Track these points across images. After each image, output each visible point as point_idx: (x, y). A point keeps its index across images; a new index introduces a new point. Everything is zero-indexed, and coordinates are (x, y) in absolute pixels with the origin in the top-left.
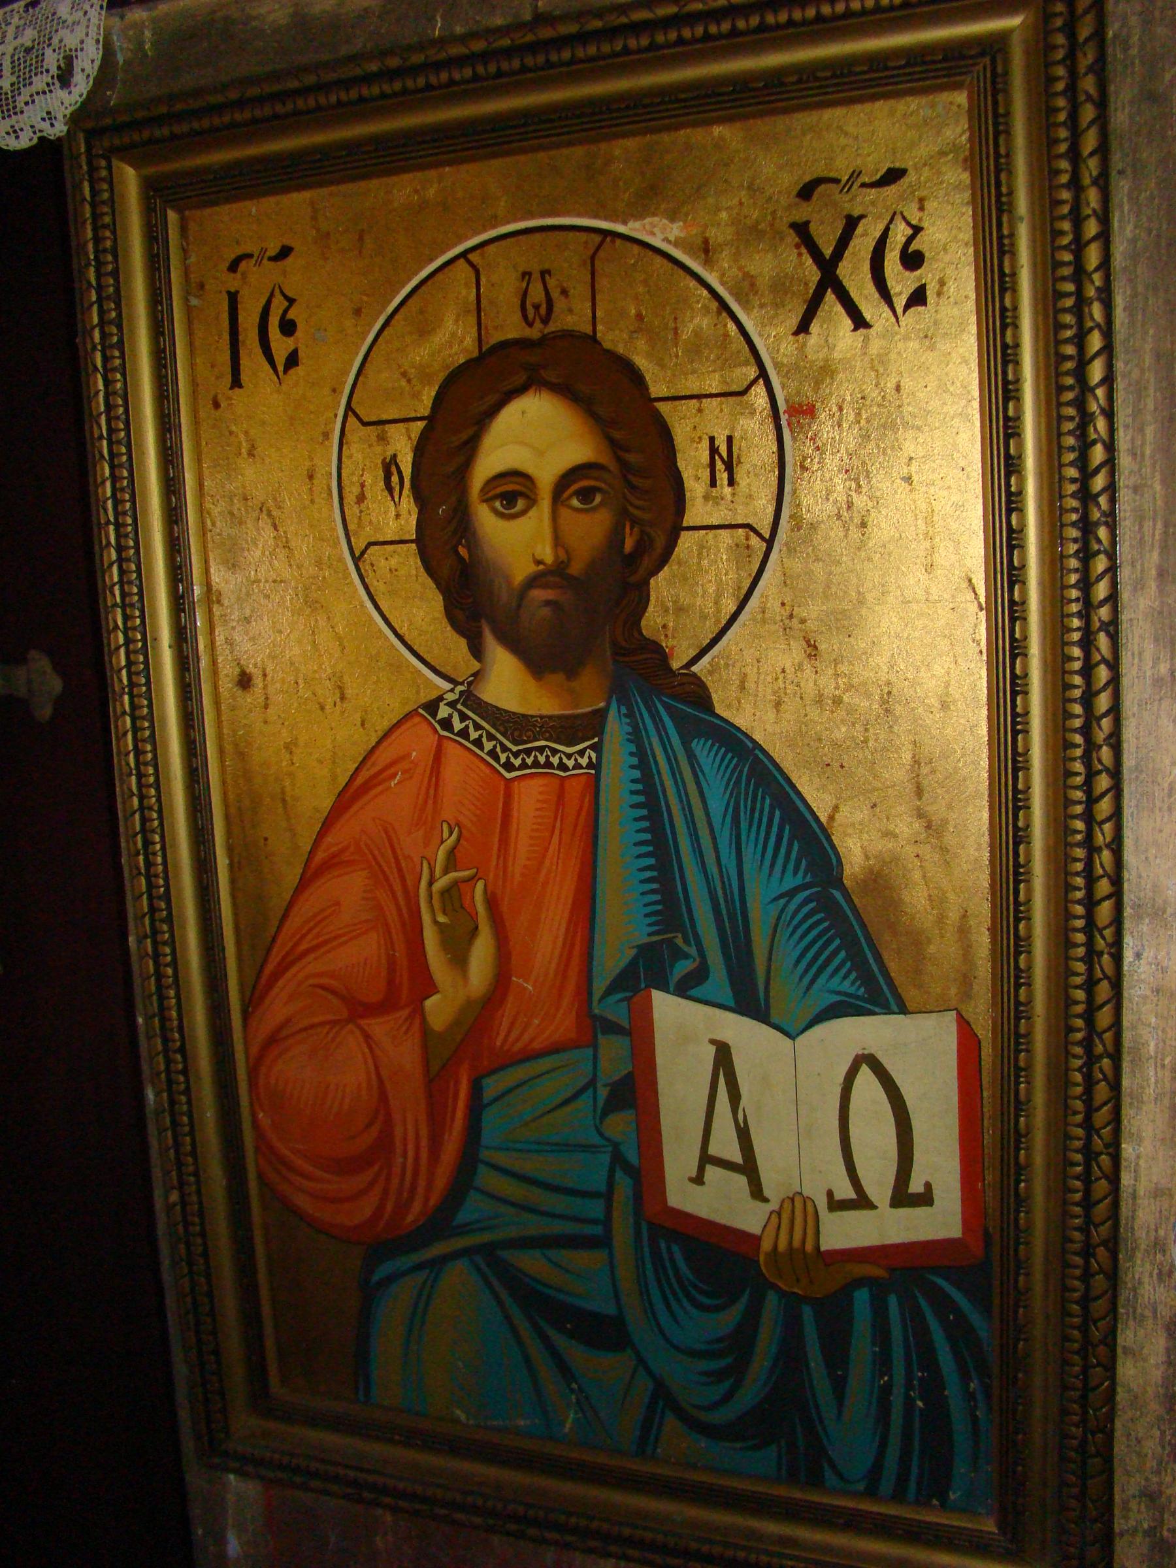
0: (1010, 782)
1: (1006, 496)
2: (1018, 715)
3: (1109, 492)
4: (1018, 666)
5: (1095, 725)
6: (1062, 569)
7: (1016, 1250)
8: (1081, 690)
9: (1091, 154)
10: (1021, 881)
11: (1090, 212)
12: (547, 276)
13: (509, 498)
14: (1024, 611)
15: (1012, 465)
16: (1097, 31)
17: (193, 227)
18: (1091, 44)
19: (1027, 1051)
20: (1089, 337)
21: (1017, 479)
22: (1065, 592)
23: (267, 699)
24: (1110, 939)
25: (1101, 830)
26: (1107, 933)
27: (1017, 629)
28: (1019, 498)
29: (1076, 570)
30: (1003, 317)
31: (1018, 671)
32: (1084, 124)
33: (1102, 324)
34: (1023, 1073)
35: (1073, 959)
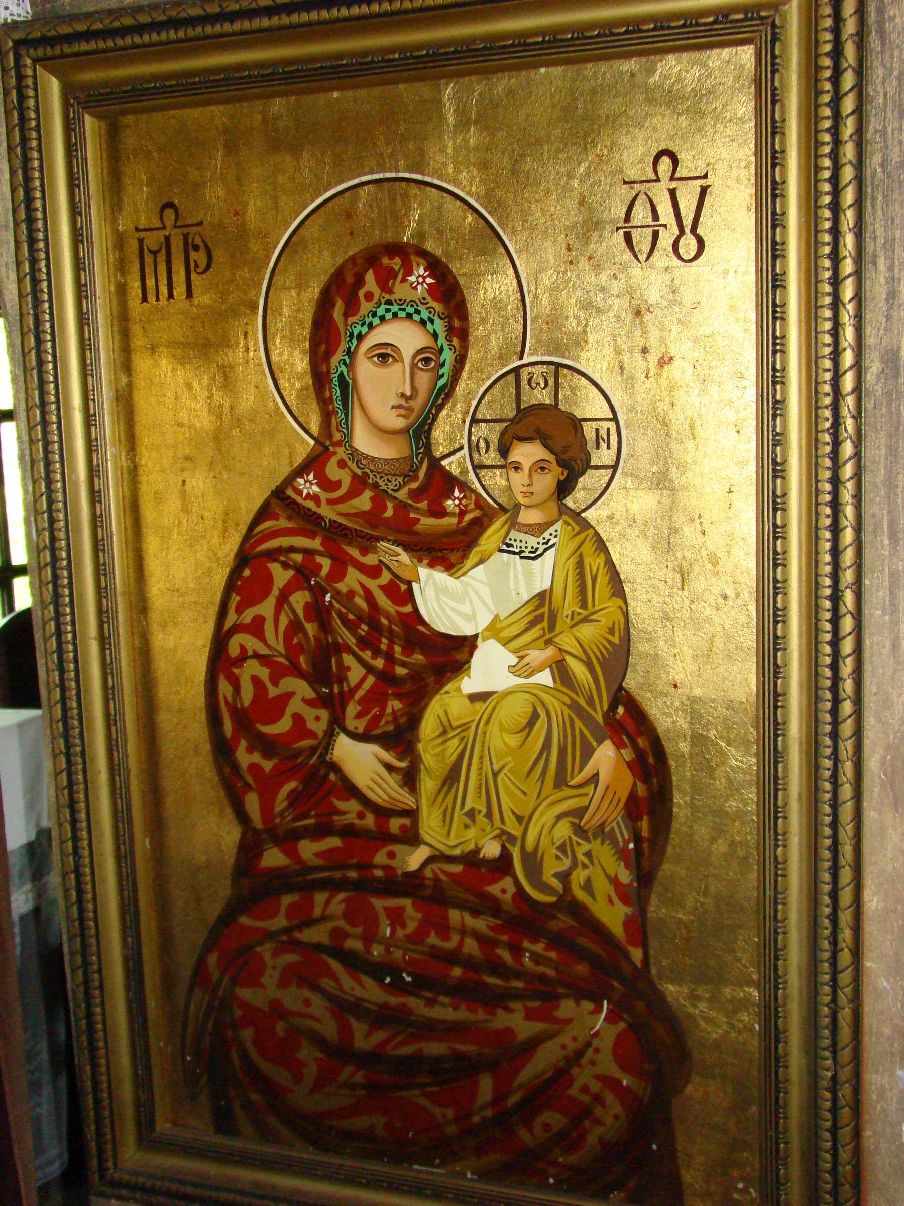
0: (772, 771)
1: (772, 184)
2: (779, 609)
3: (856, 458)
4: (778, 206)
5: (841, 662)
6: (816, 292)
7: (777, 1072)
8: (830, 95)
9: (849, 207)
10: (779, 649)
11: (846, 345)
12: (408, 393)
13: (384, 357)
14: (785, 701)
15: (777, 221)
16: (857, 108)
17: (130, 140)
18: (851, 209)
19: (784, 735)
20: (843, 193)
21: (782, 569)
22: (819, 411)
23: (220, 450)
24: (850, 995)
25: (844, 829)
26: (848, 990)
27: (778, 265)
28: (784, 500)
29: (829, 295)
30: (776, 783)
31: (778, 239)
32: (843, 183)
33: (854, 162)
34: (782, 1110)
35: (821, 711)
